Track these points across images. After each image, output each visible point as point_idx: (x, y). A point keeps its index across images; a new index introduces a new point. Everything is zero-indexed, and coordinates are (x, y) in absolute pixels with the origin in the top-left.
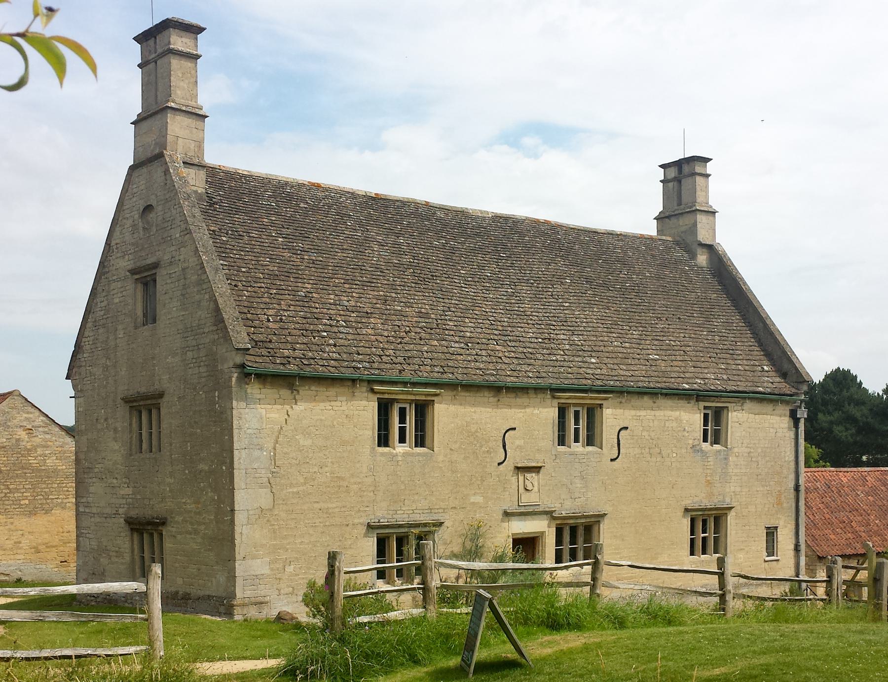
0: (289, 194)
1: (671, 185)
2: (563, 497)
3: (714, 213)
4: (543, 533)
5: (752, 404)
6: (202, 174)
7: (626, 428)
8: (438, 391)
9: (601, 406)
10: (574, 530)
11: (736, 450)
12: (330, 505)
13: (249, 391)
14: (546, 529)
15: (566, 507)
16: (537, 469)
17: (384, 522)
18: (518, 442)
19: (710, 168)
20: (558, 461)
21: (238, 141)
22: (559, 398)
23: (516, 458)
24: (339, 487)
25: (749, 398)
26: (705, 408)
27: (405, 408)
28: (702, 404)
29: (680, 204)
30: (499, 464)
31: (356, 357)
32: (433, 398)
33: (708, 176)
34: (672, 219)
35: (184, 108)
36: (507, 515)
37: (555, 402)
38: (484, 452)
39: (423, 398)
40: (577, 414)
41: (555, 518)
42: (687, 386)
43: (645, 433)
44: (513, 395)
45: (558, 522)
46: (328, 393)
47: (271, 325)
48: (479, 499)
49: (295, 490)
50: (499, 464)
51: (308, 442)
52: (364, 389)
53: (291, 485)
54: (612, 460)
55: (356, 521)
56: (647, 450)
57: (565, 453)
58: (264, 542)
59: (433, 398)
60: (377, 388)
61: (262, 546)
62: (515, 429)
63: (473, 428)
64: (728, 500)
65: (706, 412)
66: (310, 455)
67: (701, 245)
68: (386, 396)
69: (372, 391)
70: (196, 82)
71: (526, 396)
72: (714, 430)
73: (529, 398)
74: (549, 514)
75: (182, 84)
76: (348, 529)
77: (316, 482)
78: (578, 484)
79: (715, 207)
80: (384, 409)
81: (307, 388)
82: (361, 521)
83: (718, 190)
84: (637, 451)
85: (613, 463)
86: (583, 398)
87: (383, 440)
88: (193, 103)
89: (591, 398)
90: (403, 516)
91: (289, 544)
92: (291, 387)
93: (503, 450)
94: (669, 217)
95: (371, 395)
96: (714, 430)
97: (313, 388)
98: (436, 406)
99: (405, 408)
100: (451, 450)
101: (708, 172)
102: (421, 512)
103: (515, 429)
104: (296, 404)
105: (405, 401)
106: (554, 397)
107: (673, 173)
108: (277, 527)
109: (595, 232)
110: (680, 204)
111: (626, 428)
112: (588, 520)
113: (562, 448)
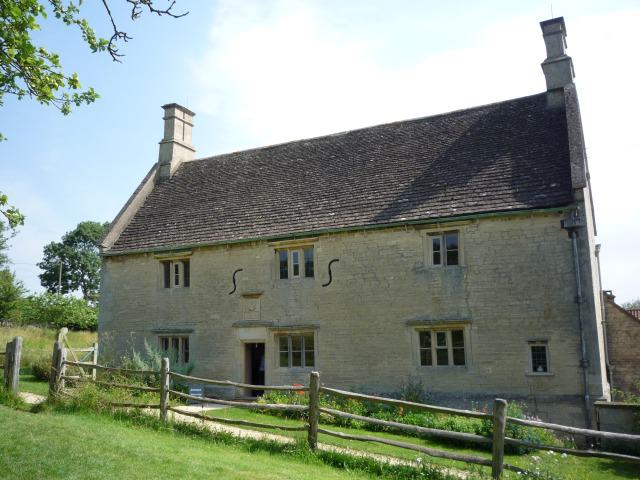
14: (266, 338)
18: (244, 279)
28: (424, 232)
36: (236, 326)
74: (270, 326)
78: (293, 304)
84: (350, 277)
90: (172, 325)
99: (438, 240)
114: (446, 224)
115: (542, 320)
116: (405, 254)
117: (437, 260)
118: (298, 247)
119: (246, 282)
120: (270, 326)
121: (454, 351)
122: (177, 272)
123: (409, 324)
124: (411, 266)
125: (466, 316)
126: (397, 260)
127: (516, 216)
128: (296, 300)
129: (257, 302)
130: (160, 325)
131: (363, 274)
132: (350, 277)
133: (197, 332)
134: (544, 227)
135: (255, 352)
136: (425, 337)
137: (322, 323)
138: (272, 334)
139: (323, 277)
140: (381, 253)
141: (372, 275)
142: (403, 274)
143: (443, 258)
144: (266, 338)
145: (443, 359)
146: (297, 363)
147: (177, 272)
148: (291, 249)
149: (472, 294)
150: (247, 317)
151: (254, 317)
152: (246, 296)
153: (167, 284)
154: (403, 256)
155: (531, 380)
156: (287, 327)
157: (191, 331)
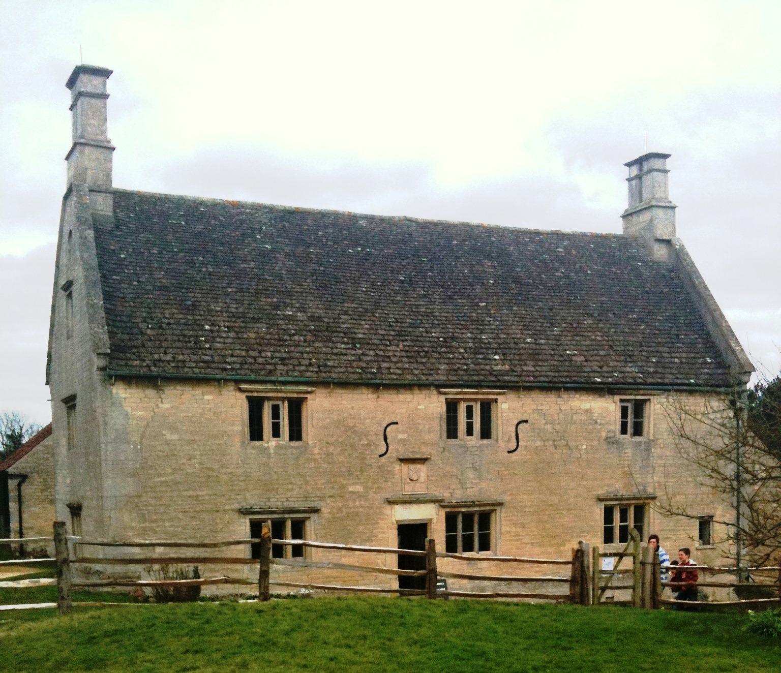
0: (202, 213)
1: (634, 182)
2: (453, 487)
3: (674, 208)
4: (431, 520)
5: (603, 399)
6: (110, 200)
7: (526, 421)
8: (309, 389)
9: (496, 400)
10: (468, 519)
11: (660, 441)
12: (200, 493)
13: (114, 391)
14: (435, 517)
15: (457, 495)
16: (423, 461)
17: (257, 508)
18: (400, 436)
19: (669, 164)
20: (446, 453)
21: (139, 169)
22: (445, 393)
23: (396, 450)
24: (209, 477)
25: (686, 391)
26: (622, 401)
27: (627, 407)
28: (617, 398)
29: (641, 201)
30: (380, 456)
31: (229, 360)
32: (305, 396)
33: (666, 172)
34: (634, 216)
35: (92, 143)
36: (391, 502)
37: (442, 398)
38: (363, 445)
39: (295, 395)
40: (470, 410)
41: (444, 507)
42: (598, 380)
43: (549, 427)
44: (395, 392)
45: (448, 510)
46: (193, 392)
47: (149, 331)
48: (359, 488)
49: (163, 479)
50: (380, 456)
51: (175, 437)
52: (232, 388)
53: (159, 475)
54: (509, 452)
55: (227, 507)
56: (551, 442)
57: (454, 445)
58: (133, 524)
59: (305, 396)
60: (243, 386)
61: (132, 528)
62: (397, 423)
63: (351, 423)
64: (650, 490)
65: (625, 404)
66: (179, 448)
67: (659, 241)
68: (255, 394)
69: (240, 390)
70: (106, 119)
71: (409, 392)
72: (634, 421)
73: (413, 394)
74: (439, 502)
75: (92, 121)
76: (218, 514)
77: (184, 472)
78: (470, 474)
79: (674, 203)
80: (255, 406)
81: (172, 387)
82: (233, 507)
83: (676, 186)
84: (539, 443)
85: (511, 454)
86: (477, 393)
87: (256, 434)
88: (100, 138)
89: (483, 394)
90: (277, 502)
91: (158, 526)
92: (156, 387)
93: (384, 443)
94: (631, 214)
95: (238, 394)
96: (634, 421)
97: (178, 387)
98: (310, 402)
99: (627, 407)
100: (328, 443)
101: (667, 168)
102: (295, 500)
103: (397, 423)
104: (162, 403)
105: (278, 399)
106: (440, 393)
107: (635, 171)
108: (146, 512)
109: (538, 233)
110: (641, 201)
111: (526, 421)
112: (482, 508)
113: (452, 441)
114: (642, 392)
115: (710, 496)
116: (599, 421)
117: (624, 431)
118: (475, 400)
119: (403, 441)
120: (439, 502)
121: (480, 535)
122: (470, 414)
123: (600, 500)
124: (604, 434)
125: (652, 491)
126: (590, 427)
127: (696, 391)
128: (475, 469)
129: (422, 471)
130: (253, 500)
131: (554, 441)
132: (539, 443)
133: (324, 510)
134: (54, 426)
135: (412, 534)
136: (256, 528)
137: (506, 498)
138: (442, 513)
139: (509, 440)
140: (574, 417)
141: (564, 443)
142: (595, 443)
143: (630, 429)
144: (435, 517)
145: (624, 536)
146: (468, 547)
147: (470, 414)
148: (465, 400)
149: (657, 469)
150: (409, 490)
151: (419, 489)
152: (403, 461)
153: (452, 433)
154: (596, 422)
155: (699, 553)
156: (457, 505)
157: (316, 511)
